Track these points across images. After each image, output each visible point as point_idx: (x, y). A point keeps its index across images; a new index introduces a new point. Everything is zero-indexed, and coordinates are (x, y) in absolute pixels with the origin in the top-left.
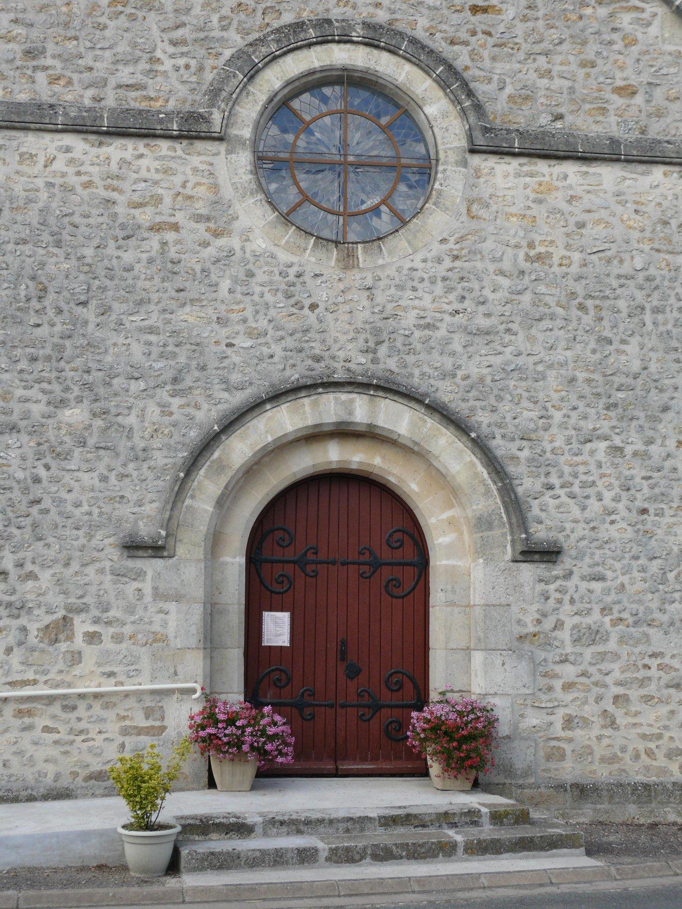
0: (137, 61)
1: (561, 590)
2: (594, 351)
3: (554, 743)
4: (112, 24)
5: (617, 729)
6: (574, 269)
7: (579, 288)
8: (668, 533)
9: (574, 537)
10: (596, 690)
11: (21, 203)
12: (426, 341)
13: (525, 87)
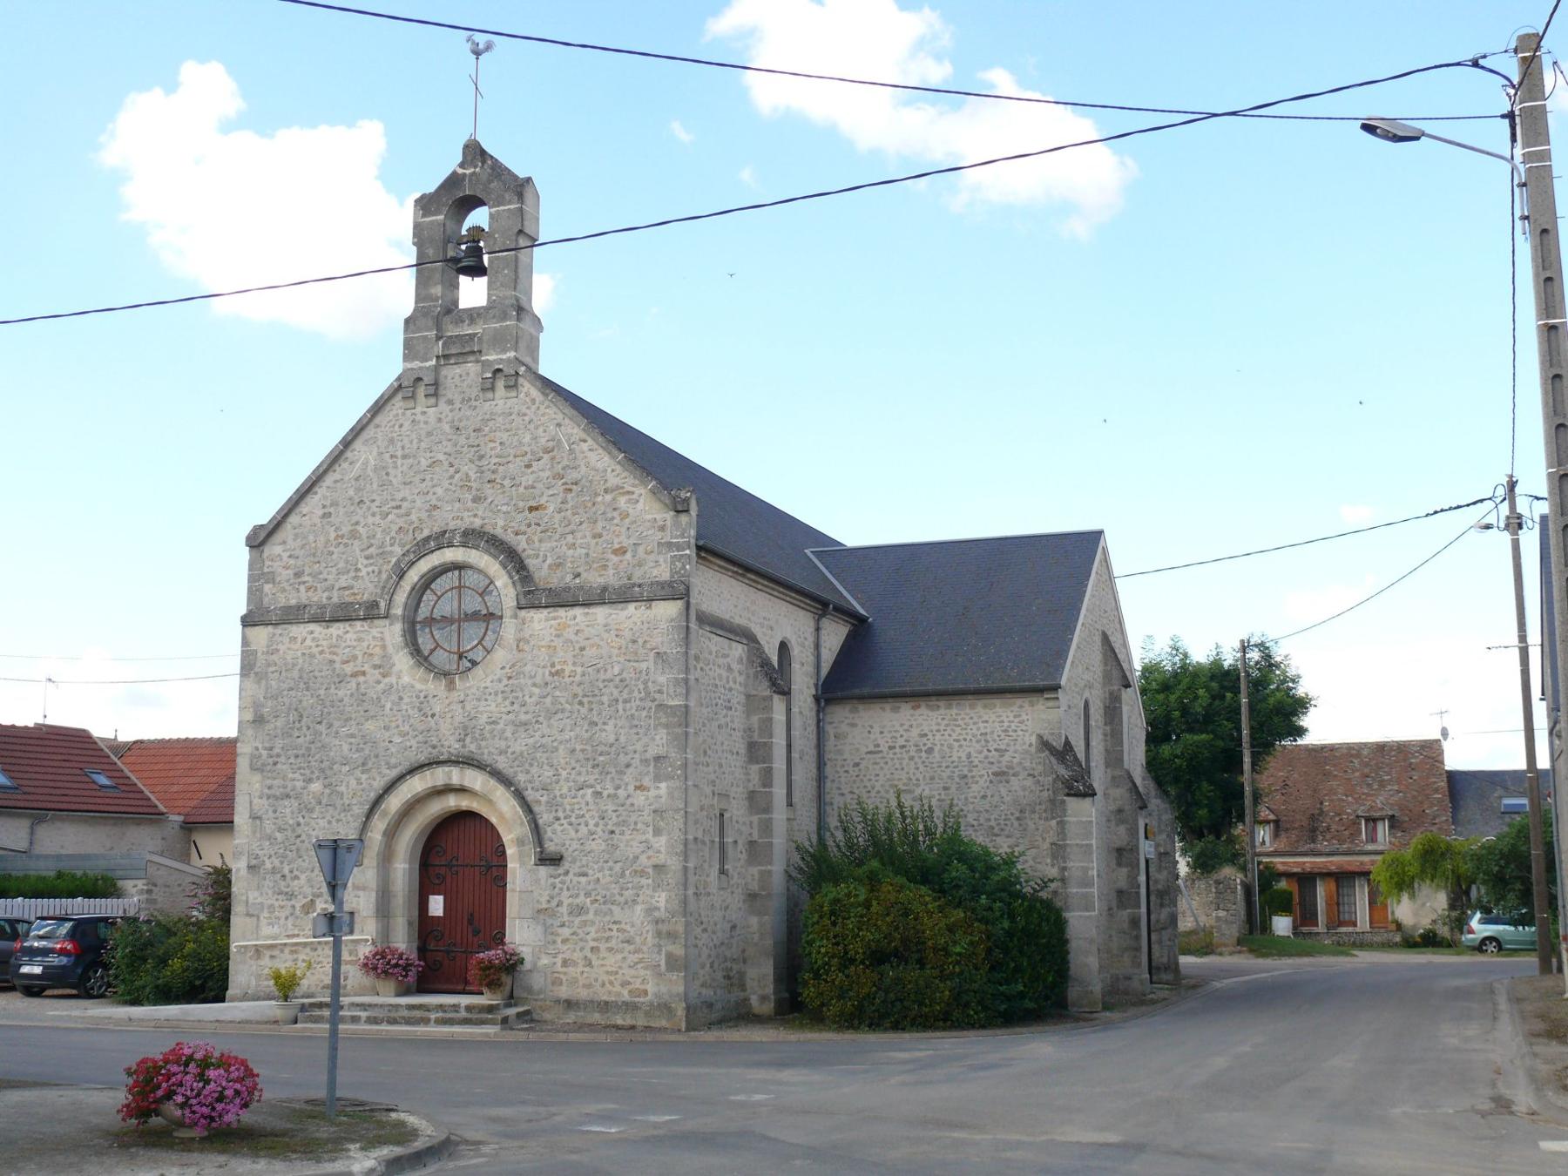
0: (348, 572)
1: (563, 883)
2: (587, 731)
3: (556, 975)
4: (336, 550)
5: (592, 967)
6: (578, 678)
7: (579, 691)
8: (626, 846)
9: (571, 849)
10: (581, 944)
11: (290, 667)
12: (491, 732)
13: (559, 557)
